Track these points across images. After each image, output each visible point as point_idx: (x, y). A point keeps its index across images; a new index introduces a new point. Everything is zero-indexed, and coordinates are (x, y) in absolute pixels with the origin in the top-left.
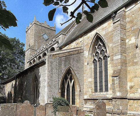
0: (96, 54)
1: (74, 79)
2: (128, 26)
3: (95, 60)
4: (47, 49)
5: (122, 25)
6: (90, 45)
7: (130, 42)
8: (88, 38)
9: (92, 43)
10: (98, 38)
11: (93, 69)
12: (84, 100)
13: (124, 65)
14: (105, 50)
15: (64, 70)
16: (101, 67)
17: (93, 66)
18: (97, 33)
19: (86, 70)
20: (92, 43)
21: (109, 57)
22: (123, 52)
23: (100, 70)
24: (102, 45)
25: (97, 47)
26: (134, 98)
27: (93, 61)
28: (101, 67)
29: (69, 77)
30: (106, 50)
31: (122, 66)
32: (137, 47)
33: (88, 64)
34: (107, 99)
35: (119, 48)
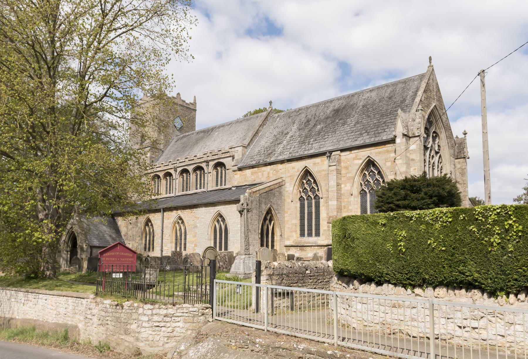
0: (303, 190)
1: (274, 220)
2: (343, 172)
3: (301, 197)
4: (207, 162)
5: (338, 170)
6: (296, 178)
7: (346, 188)
8: (293, 168)
9: (299, 176)
10: (307, 173)
11: (299, 209)
12: (286, 246)
13: (339, 211)
14: (316, 188)
15: (264, 208)
16: (310, 206)
17: (298, 205)
18: (306, 167)
19: (289, 209)
20: (299, 176)
21: (322, 198)
22: (339, 198)
23: (308, 210)
24: (312, 181)
25: (305, 181)
26: (299, 245)
27: (300, 198)
28: (310, 206)
29: (268, 218)
30: (318, 189)
31: (338, 212)
32: (352, 195)
33: (292, 201)
34: (318, 246)
35: (335, 194)
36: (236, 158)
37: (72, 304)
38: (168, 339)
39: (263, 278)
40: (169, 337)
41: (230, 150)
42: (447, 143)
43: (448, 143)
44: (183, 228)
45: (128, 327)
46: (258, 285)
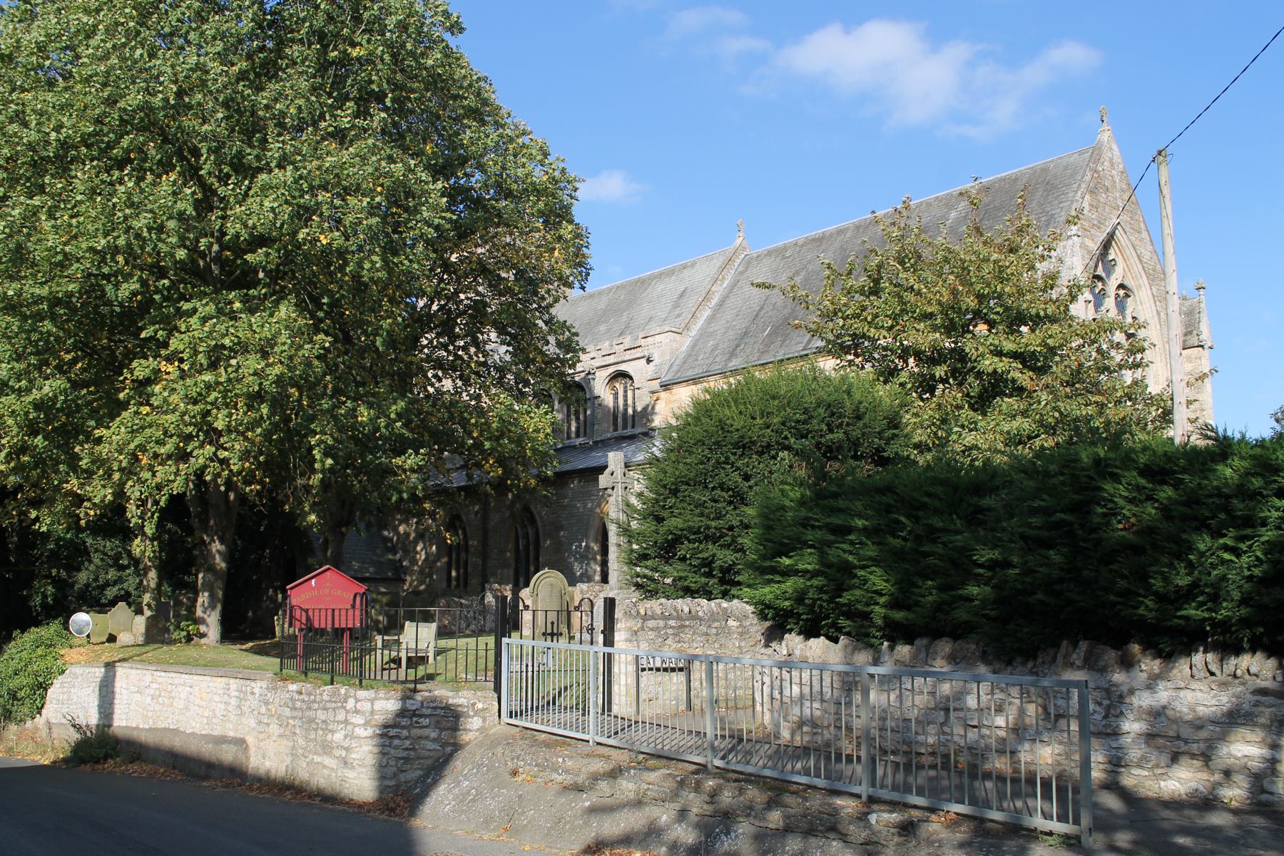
36: (656, 357)
37: (237, 694)
38: (404, 764)
39: (619, 636)
40: (406, 759)
41: (643, 342)
42: (1155, 313)
43: (1158, 313)
44: (530, 531)
45: (329, 736)
46: (608, 650)
